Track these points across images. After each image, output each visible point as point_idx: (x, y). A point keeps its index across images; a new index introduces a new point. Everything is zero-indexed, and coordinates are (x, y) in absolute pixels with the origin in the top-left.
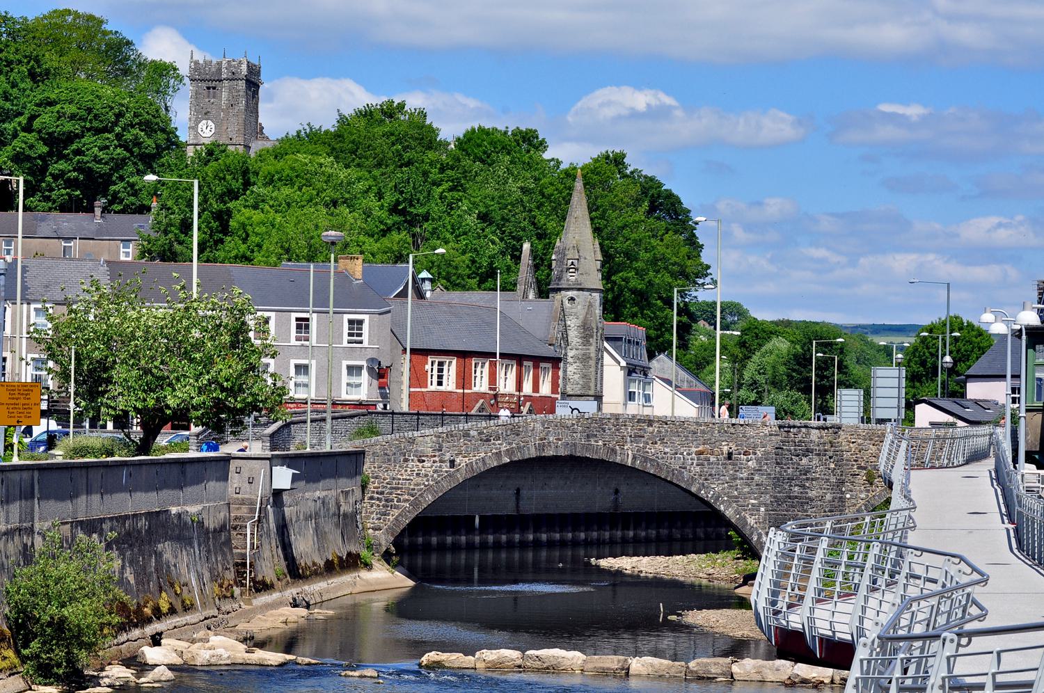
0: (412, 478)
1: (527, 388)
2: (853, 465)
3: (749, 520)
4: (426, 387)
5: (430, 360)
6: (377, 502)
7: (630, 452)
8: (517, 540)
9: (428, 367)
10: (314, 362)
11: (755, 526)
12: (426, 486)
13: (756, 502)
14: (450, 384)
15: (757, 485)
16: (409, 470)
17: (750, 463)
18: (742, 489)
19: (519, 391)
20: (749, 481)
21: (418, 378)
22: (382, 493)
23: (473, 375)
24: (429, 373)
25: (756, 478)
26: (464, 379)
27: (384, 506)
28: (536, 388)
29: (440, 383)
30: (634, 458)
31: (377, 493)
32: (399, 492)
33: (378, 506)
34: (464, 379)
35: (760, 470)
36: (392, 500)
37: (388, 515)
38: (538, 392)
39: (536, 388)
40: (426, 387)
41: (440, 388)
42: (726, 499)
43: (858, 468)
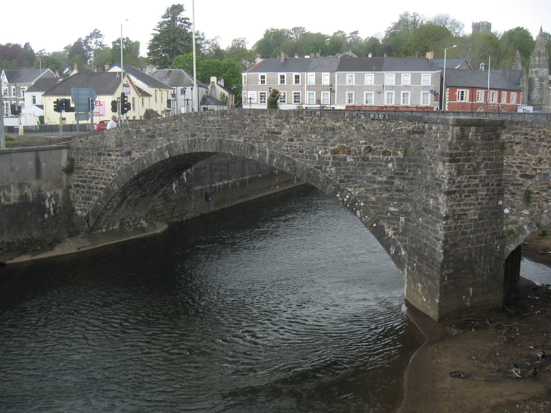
0: (104, 169)
1: (504, 101)
2: (515, 172)
3: (387, 230)
4: (456, 101)
5: (458, 90)
6: (82, 190)
7: (268, 150)
8: (374, 200)
9: (457, 93)
10: (409, 92)
11: (393, 237)
12: (113, 177)
13: (396, 210)
14: (466, 100)
15: (397, 191)
16: (102, 162)
17: (390, 165)
18: (381, 194)
19: (472, 101)
20: (388, 186)
21: (452, 97)
22: (85, 181)
23: (477, 96)
24: (457, 96)
25: (397, 182)
26: (473, 97)
27: (88, 192)
28: (508, 100)
29: (462, 99)
30: (271, 156)
31: (81, 181)
32: (96, 181)
33: (83, 192)
34: (473, 97)
35: (402, 174)
36: (93, 188)
37: (91, 200)
38: (509, 103)
39: (508, 100)
40: (456, 101)
41: (462, 101)
42: (362, 204)
43: (522, 176)
